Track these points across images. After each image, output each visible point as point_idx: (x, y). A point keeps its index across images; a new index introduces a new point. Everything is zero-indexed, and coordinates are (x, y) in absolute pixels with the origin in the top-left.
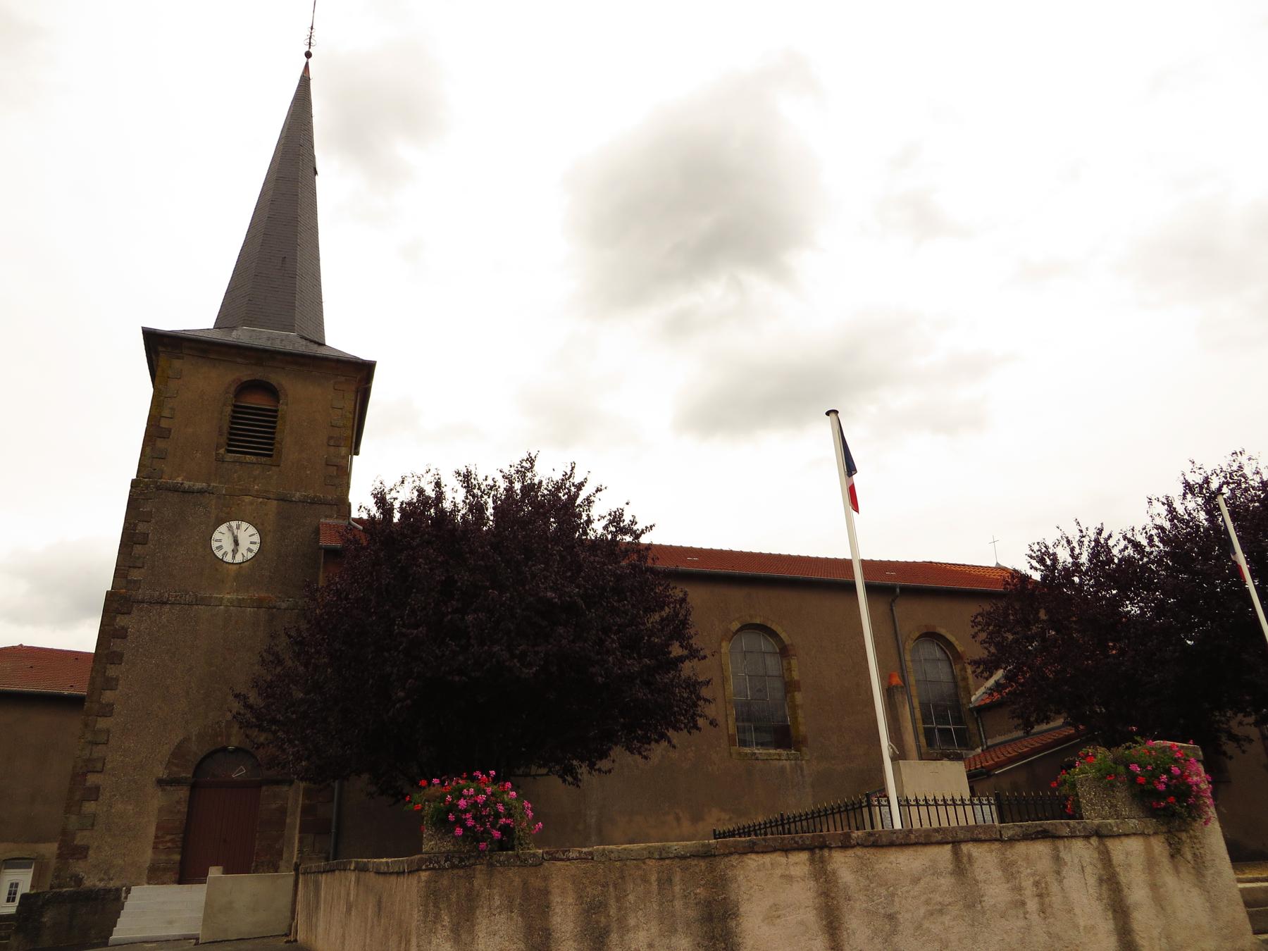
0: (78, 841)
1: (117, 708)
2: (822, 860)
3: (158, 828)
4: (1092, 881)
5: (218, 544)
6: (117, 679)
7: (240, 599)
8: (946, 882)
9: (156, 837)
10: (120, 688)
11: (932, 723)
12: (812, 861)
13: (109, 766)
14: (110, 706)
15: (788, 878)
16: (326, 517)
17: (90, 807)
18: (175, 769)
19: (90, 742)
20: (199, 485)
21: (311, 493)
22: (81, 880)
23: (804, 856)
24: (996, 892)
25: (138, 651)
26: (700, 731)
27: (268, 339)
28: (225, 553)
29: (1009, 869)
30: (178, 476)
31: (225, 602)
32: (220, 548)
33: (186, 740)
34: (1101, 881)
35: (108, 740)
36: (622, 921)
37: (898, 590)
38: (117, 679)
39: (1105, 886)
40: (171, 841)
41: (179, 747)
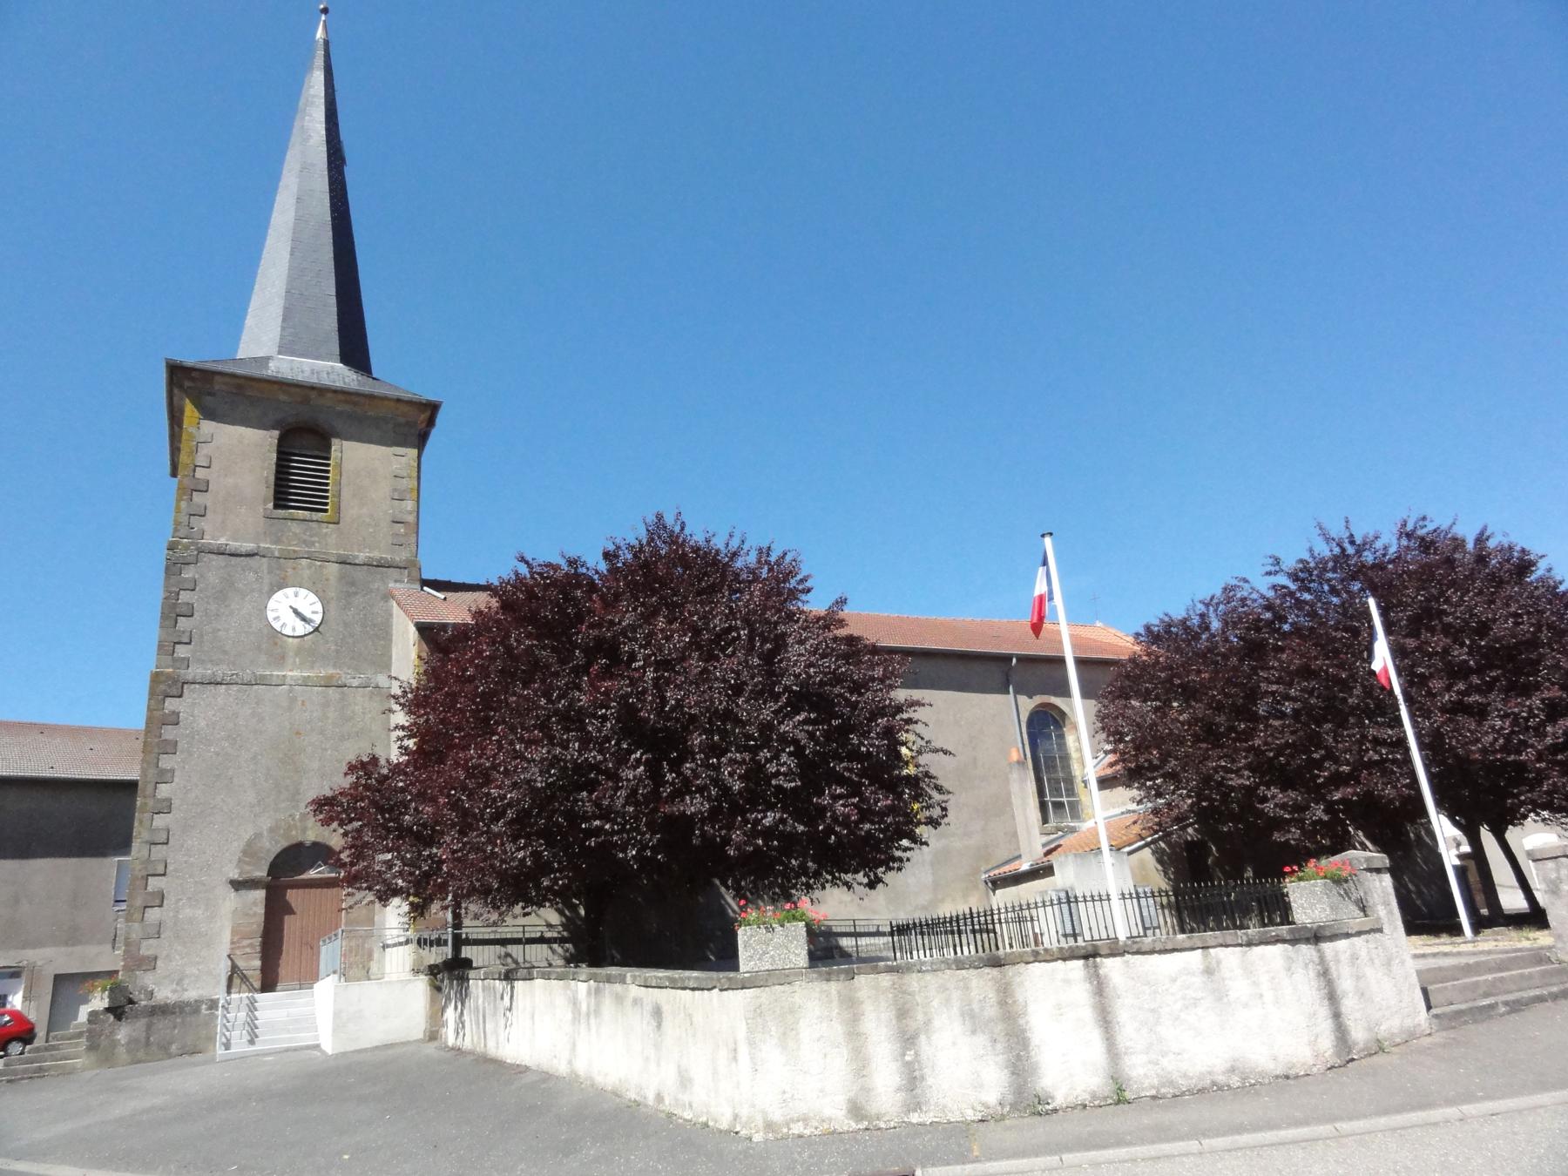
0: (144, 952)
1: (176, 803)
2: (1096, 966)
3: (234, 932)
4: (1312, 974)
5: (275, 615)
6: (173, 771)
7: (304, 677)
8: (1198, 980)
9: (232, 943)
10: (176, 780)
11: (1068, 802)
12: (1086, 966)
13: (170, 868)
14: (169, 800)
15: (1067, 981)
16: (396, 581)
17: (153, 915)
18: (248, 868)
19: (146, 842)
20: (249, 546)
21: (376, 554)
22: (152, 993)
23: (1081, 962)
24: (1239, 987)
25: (193, 738)
26: (928, 845)
27: (312, 372)
28: (284, 625)
29: (1248, 971)
30: (222, 536)
31: (288, 681)
32: (277, 618)
33: (258, 836)
34: (1319, 975)
35: (168, 839)
36: (928, 1022)
37: (1014, 660)
38: (173, 771)
39: (1322, 978)
40: (251, 945)
41: (249, 844)
